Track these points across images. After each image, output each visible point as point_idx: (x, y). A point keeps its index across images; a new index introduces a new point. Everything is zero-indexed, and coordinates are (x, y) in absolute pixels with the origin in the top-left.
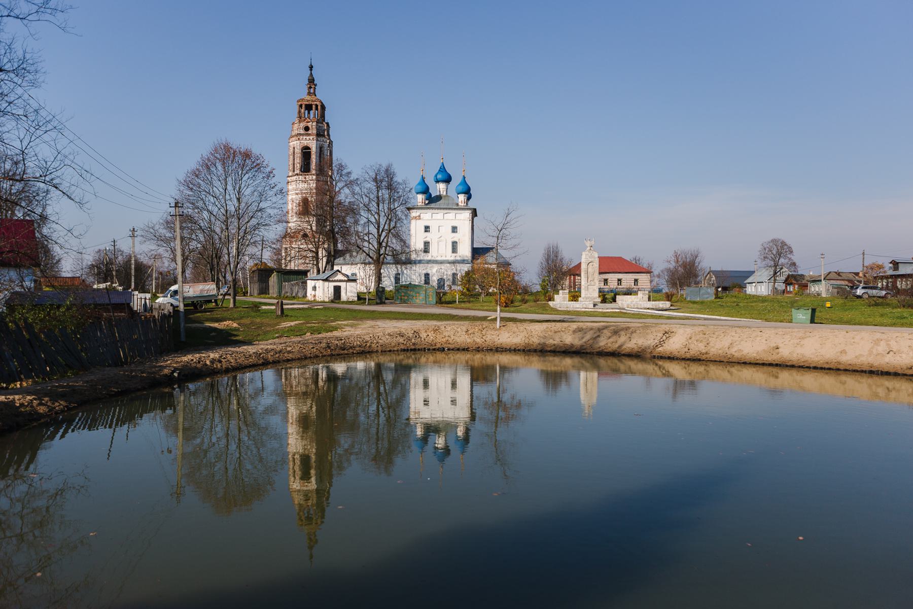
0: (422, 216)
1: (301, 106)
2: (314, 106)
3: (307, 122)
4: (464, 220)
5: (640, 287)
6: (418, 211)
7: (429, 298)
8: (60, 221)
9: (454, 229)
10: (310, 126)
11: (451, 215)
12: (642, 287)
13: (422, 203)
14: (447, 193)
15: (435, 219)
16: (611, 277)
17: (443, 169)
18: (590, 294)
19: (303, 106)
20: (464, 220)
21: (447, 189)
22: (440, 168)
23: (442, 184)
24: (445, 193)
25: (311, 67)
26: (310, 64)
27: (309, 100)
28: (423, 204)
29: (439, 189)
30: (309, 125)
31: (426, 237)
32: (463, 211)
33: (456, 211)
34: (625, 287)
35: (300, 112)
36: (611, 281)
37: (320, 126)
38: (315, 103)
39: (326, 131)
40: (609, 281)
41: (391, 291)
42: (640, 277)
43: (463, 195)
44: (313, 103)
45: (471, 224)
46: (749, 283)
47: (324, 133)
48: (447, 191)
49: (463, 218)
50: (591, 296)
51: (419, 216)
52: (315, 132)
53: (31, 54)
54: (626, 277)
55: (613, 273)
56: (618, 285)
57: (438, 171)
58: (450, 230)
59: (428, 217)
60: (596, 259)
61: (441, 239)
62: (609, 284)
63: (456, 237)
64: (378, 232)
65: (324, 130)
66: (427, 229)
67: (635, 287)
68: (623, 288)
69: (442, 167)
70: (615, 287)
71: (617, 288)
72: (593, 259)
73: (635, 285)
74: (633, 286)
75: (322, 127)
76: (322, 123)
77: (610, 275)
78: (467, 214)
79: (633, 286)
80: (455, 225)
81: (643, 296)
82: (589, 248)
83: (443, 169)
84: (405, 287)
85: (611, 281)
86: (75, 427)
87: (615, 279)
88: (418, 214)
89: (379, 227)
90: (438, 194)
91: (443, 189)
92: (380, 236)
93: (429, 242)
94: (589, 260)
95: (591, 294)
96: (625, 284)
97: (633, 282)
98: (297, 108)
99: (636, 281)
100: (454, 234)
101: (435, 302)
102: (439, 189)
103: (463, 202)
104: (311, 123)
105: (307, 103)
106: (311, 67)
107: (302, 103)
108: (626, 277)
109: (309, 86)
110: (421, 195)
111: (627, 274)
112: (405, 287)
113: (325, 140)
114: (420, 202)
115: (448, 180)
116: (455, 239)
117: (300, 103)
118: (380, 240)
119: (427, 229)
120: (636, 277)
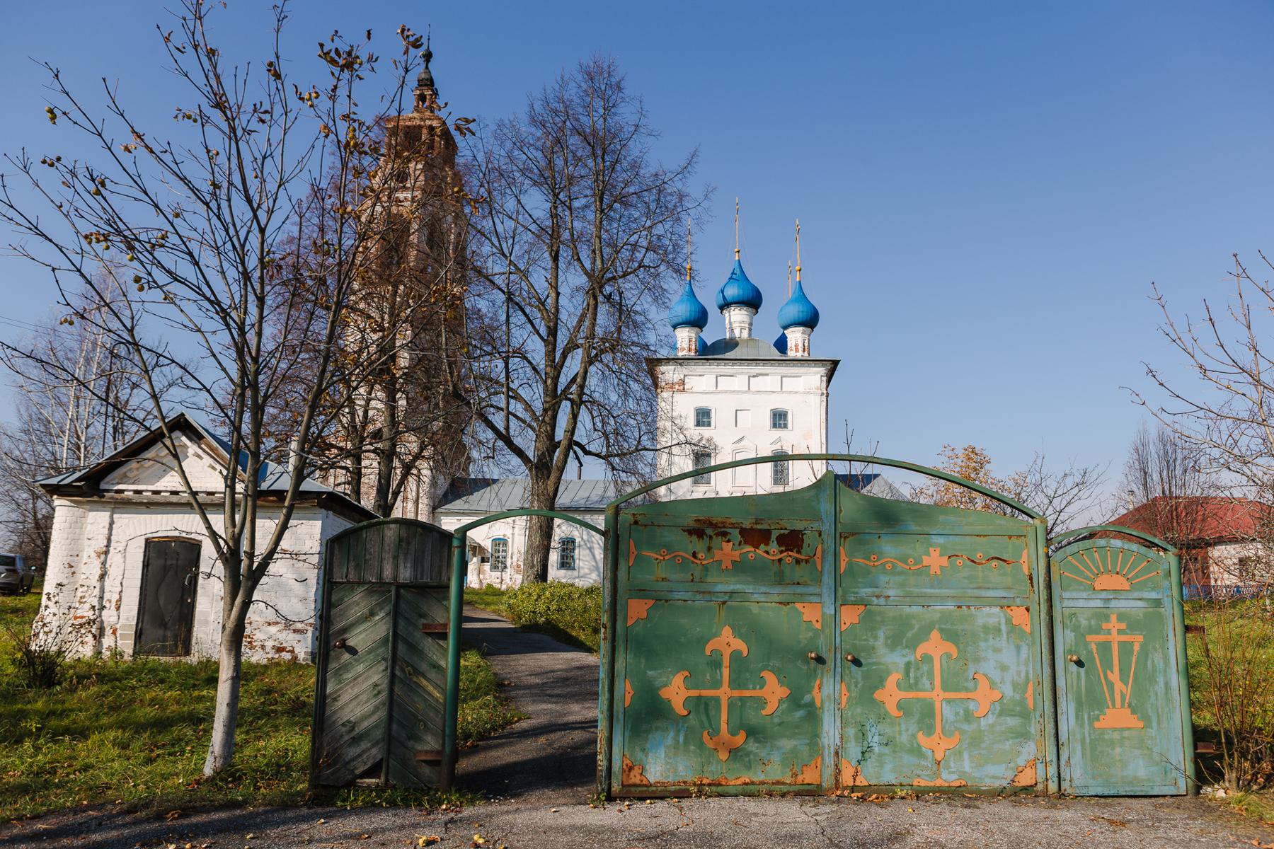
0: (690, 383)
7: (1092, 701)
8: (306, 549)
14: (750, 334)
17: (739, 276)
21: (751, 324)
22: (733, 273)
23: (737, 311)
24: (745, 335)
29: (730, 323)
38: (428, 123)
41: (590, 591)
43: (801, 329)
48: (750, 330)
49: (801, 389)
51: (683, 383)
57: (727, 280)
61: (742, 443)
64: (551, 353)
69: (738, 271)
78: (815, 376)
80: (780, 405)
83: (739, 276)
84: (757, 536)
86: (100, 825)
89: (553, 332)
90: (728, 337)
92: (558, 369)
100: (778, 433)
101: (1180, 754)
102: (730, 323)
103: (801, 349)
109: (418, 92)
110: (687, 329)
112: (757, 536)
115: (753, 302)
118: (556, 380)
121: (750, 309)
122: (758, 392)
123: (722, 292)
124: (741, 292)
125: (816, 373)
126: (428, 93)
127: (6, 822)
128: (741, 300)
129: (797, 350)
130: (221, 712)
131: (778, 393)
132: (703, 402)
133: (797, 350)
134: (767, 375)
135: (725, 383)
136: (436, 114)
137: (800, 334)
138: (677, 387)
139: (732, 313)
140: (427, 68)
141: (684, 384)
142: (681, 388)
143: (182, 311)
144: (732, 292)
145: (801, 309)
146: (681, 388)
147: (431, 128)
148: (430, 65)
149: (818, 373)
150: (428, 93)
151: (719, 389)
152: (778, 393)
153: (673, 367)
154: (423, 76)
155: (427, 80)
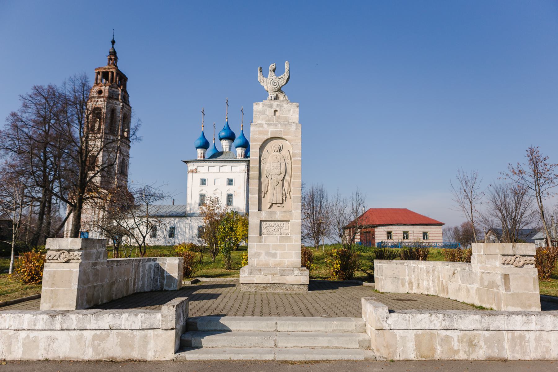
1: (98, 73)
2: (110, 73)
3: (101, 86)
4: (240, 172)
5: (432, 241)
6: (194, 164)
9: (230, 182)
10: (103, 90)
11: (227, 167)
12: (434, 241)
13: (201, 157)
15: (211, 172)
16: (395, 229)
18: (268, 254)
19: (101, 73)
20: (240, 172)
22: (225, 127)
24: (228, 150)
25: (113, 42)
26: (112, 39)
27: (106, 68)
28: (202, 158)
30: (103, 88)
31: (202, 190)
32: (238, 164)
33: (232, 164)
34: (412, 241)
35: (97, 79)
36: (395, 235)
37: (114, 91)
38: (111, 70)
39: (120, 95)
40: (393, 234)
42: (430, 230)
44: (109, 70)
45: (246, 176)
46: (537, 239)
47: (118, 97)
49: (238, 171)
50: (272, 261)
51: (196, 169)
52: (107, 95)
53: (36, 99)
54: (412, 229)
55: (397, 224)
56: (404, 238)
58: (225, 182)
59: (204, 169)
60: (293, 127)
61: (216, 191)
62: (393, 237)
63: (231, 189)
65: (119, 95)
66: (203, 182)
67: (424, 241)
68: (410, 242)
69: (226, 126)
70: (400, 241)
71: (401, 242)
72: (279, 128)
73: (424, 239)
74: (422, 240)
75: (117, 91)
76: (117, 88)
77: (394, 227)
79: (422, 240)
80: (230, 177)
81: (510, 270)
82: (272, 95)
85: (395, 235)
87: (399, 232)
88: (195, 167)
91: (226, 145)
93: (205, 195)
94: (266, 132)
95: (274, 255)
96: (413, 237)
97: (422, 235)
98: (95, 74)
99: (425, 234)
100: (230, 187)
104: (104, 87)
105: (104, 70)
106: (113, 42)
107: (100, 71)
108: (412, 229)
109: (109, 57)
110: (200, 149)
111: (414, 227)
113: (118, 103)
114: (199, 157)
115: (231, 137)
116: (231, 192)
117: (97, 71)
119: (203, 182)
120: (425, 230)
121: (229, 140)
122: (223, 172)
123: (219, 134)
124: (225, 134)
125: (244, 165)
126: (113, 57)
127: (1, 146)
128: (225, 137)
129: (239, 156)
130: (11, 268)
131: (230, 172)
132: (203, 177)
133: (239, 156)
134: (226, 166)
135: (211, 169)
136: (4, 160)
137: (240, 150)
138: (194, 171)
139: (223, 142)
140: (113, 47)
141: (197, 170)
142: (196, 171)
143: (113, 35)
144: (223, 134)
145: (240, 141)
146: (196, 171)
147: (113, 73)
148: (114, 46)
149: (244, 165)
150: (113, 57)
151: (232, 171)
152: (230, 172)
153: (193, 164)
154: (111, 50)
155: (112, 52)
